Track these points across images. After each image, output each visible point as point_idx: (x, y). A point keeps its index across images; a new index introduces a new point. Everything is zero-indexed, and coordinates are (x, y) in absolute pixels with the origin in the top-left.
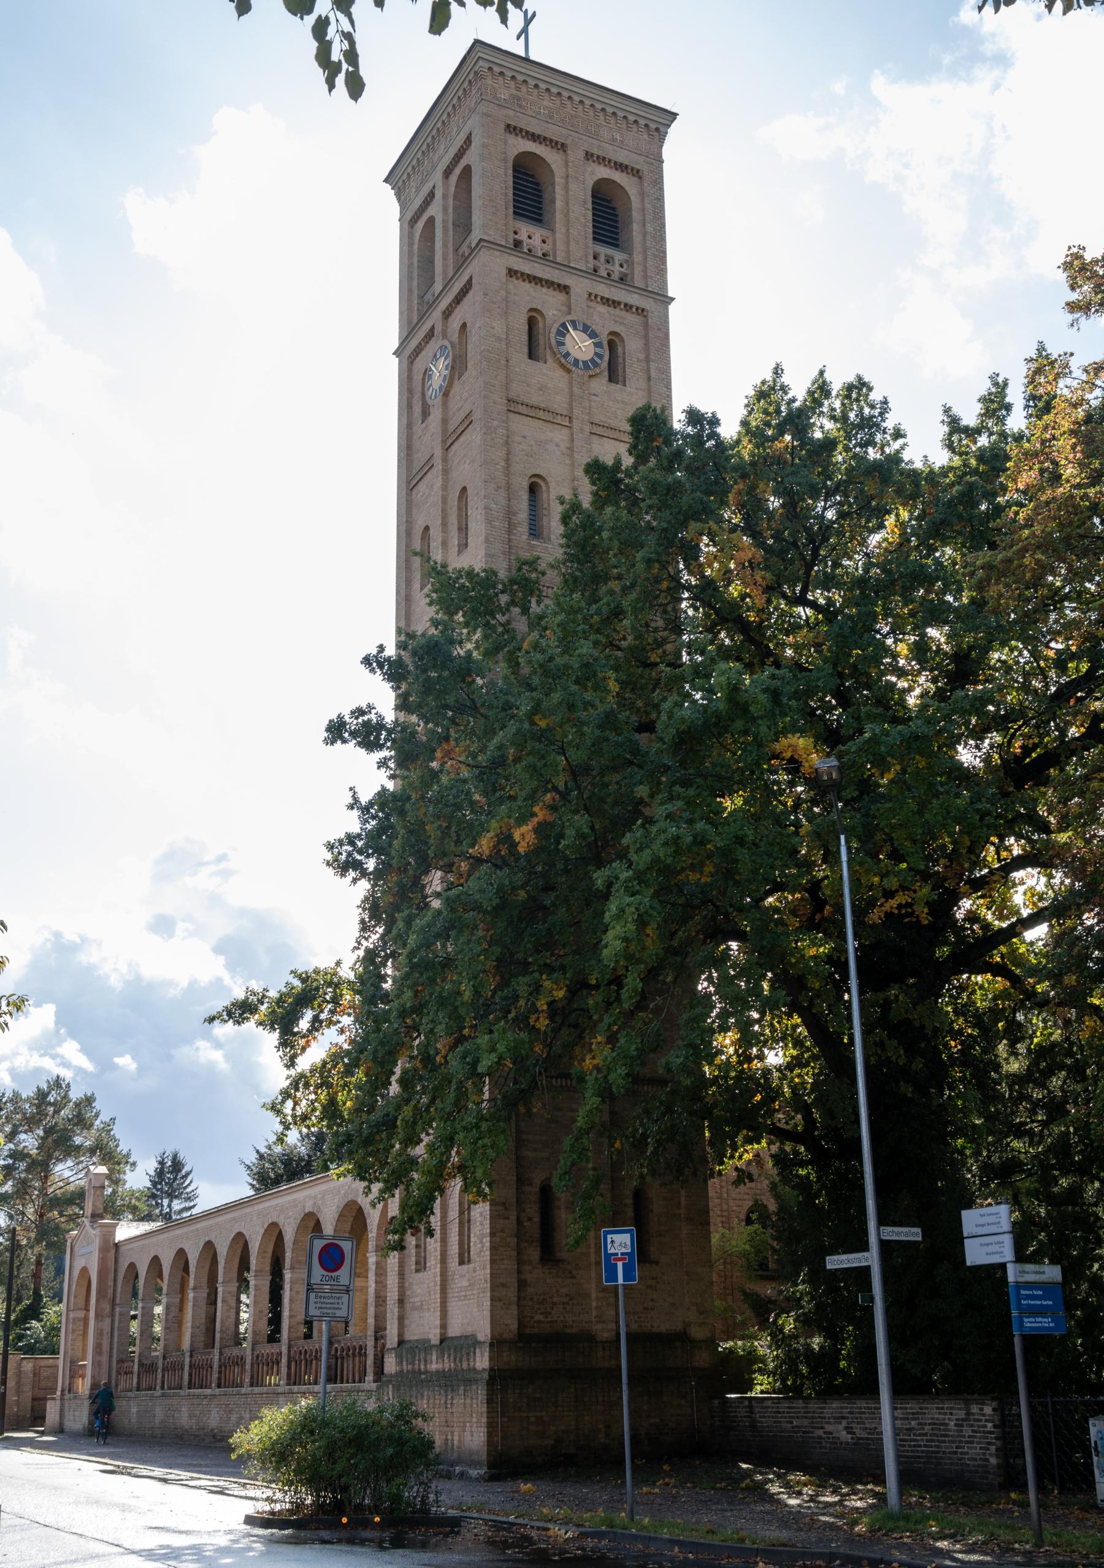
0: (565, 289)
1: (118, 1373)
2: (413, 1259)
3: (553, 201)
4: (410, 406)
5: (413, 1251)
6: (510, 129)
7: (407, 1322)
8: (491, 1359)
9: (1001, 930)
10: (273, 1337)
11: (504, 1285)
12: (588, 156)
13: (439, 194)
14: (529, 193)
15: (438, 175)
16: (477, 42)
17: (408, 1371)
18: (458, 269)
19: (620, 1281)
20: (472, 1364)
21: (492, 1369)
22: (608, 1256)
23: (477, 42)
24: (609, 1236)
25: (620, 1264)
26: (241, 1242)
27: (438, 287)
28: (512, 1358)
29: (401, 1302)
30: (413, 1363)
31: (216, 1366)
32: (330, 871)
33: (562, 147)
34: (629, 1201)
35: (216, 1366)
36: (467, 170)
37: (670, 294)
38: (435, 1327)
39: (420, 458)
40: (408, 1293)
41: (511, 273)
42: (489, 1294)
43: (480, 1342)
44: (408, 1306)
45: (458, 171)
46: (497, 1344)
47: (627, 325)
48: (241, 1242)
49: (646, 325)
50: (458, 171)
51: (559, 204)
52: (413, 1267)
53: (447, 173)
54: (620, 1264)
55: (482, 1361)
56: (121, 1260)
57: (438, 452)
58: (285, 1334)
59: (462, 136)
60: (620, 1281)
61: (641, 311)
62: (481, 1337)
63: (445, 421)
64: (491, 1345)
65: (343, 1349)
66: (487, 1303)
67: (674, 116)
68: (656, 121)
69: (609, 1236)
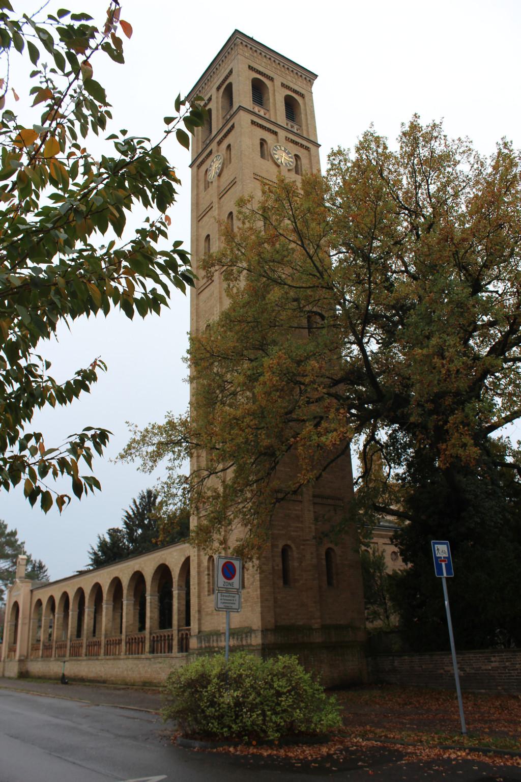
0: (275, 133)
1: (32, 650)
2: (206, 589)
3: (269, 99)
4: (198, 186)
5: (206, 585)
6: (250, 68)
7: (203, 621)
8: (262, 639)
9: (486, 427)
10: (142, 628)
11: (267, 600)
12: (283, 85)
13: (214, 98)
14: (259, 91)
15: (214, 89)
16: (236, 31)
17: (206, 647)
18: (228, 121)
19: (445, 575)
20: (249, 641)
21: (263, 644)
22: (437, 558)
23: (236, 31)
24: (436, 546)
25: (443, 564)
26: (80, 592)
27: (214, 133)
28: (271, 638)
29: (199, 611)
30: (242, 641)
31: (84, 645)
32: (408, 120)
33: (272, 79)
34: (324, 557)
35: (84, 645)
36: (230, 85)
37: (319, 143)
38: (223, 623)
39: (204, 206)
40: (203, 607)
41: (253, 123)
42: (259, 604)
43: (254, 630)
44: (203, 613)
45: (224, 86)
46: (265, 631)
47: (301, 153)
48: (80, 592)
49: (310, 154)
50: (224, 86)
51: (271, 100)
52: (206, 593)
53: (218, 88)
54: (443, 564)
55: (256, 640)
56: (33, 598)
57: (215, 200)
58: (148, 625)
59: (228, 71)
60: (445, 575)
61: (307, 149)
62: (255, 627)
63: (218, 187)
64: (262, 631)
65: (157, 637)
66: (258, 609)
67: (316, 76)
68: (310, 77)
69: (436, 546)
